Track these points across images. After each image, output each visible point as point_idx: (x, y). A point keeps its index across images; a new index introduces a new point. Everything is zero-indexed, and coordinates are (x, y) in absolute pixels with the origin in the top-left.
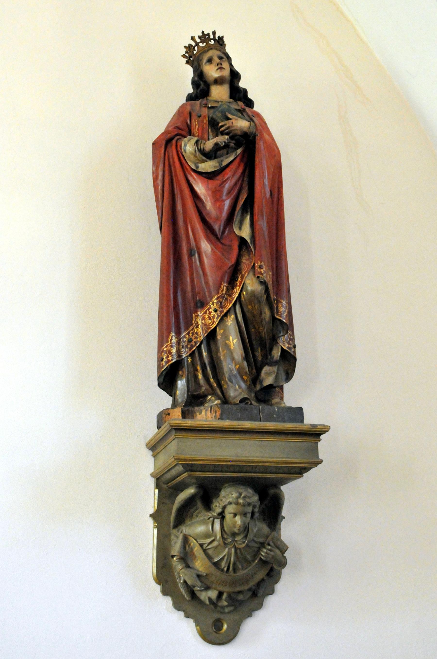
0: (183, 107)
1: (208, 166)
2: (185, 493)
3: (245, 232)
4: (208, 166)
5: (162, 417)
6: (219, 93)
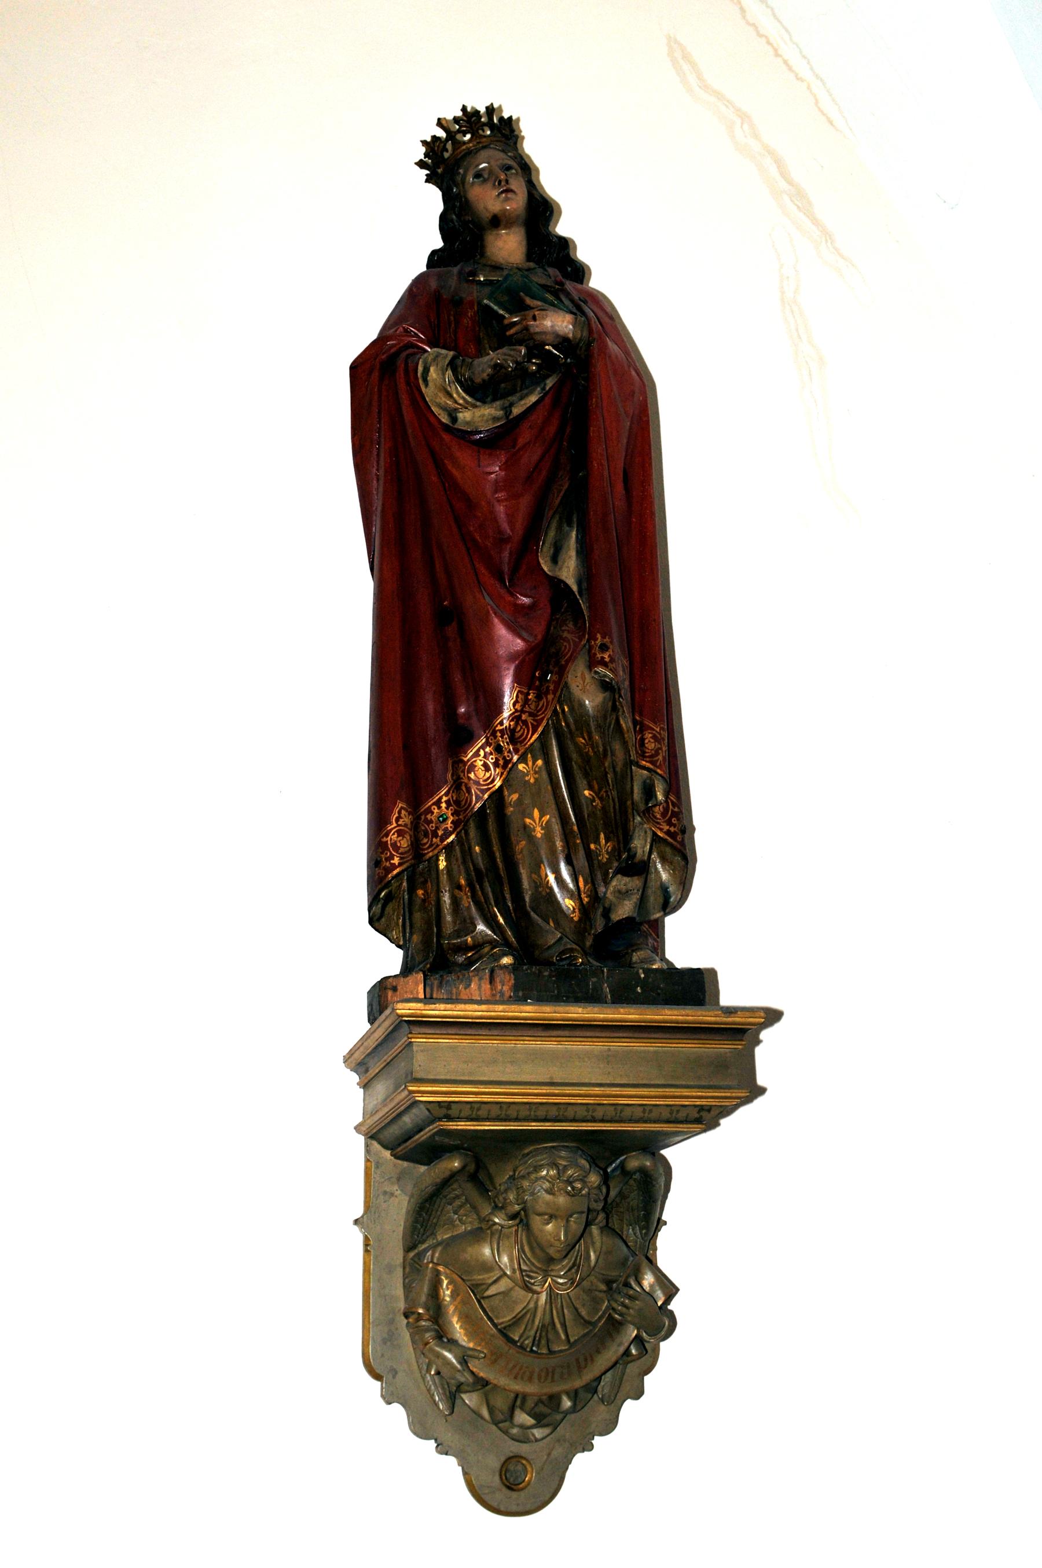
0: (419, 281)
1: (480, 417)
2: (440, 1169)
3: (569, 571)
4: (480, 417)
5: (381, 996)
6: (508, 246)
